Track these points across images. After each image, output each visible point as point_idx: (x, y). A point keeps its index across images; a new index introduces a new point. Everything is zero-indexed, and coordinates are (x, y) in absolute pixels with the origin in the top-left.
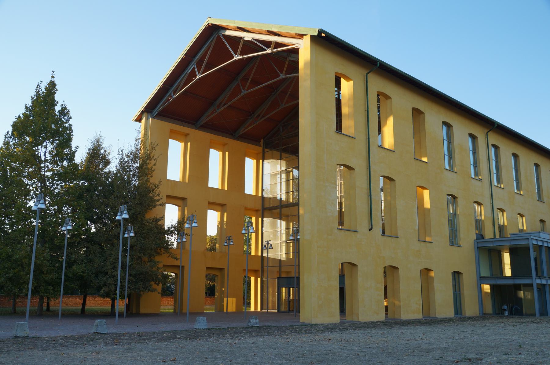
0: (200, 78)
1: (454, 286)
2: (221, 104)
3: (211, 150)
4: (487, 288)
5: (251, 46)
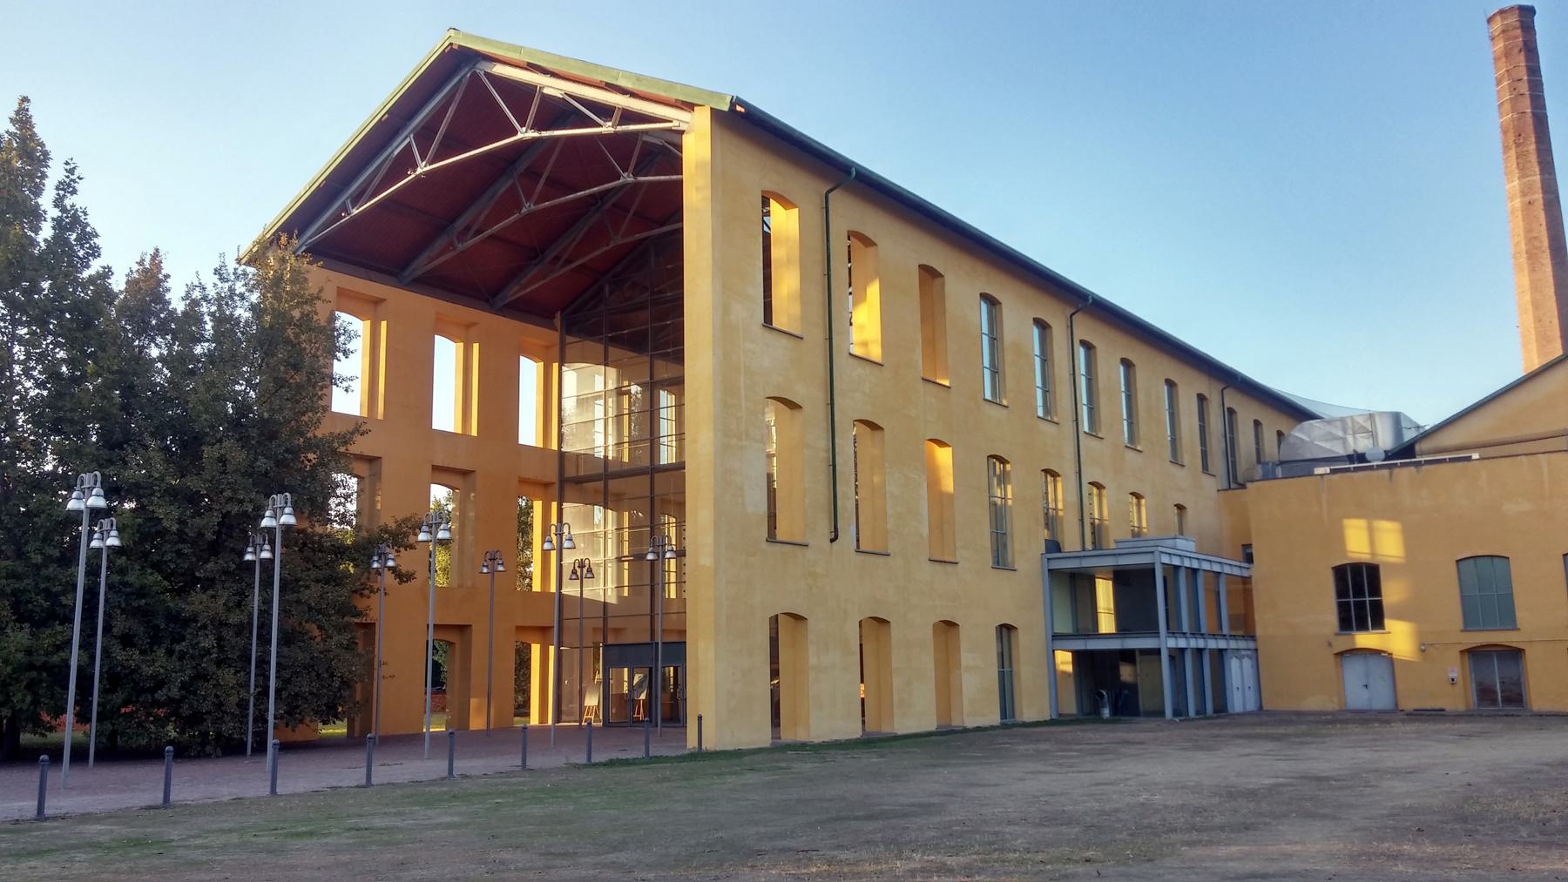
0: (427, 173)
1: (1001, 655)
2: (468, 228)
3: (437, 338)
4: (1064, 660)
5: (558, 112)
